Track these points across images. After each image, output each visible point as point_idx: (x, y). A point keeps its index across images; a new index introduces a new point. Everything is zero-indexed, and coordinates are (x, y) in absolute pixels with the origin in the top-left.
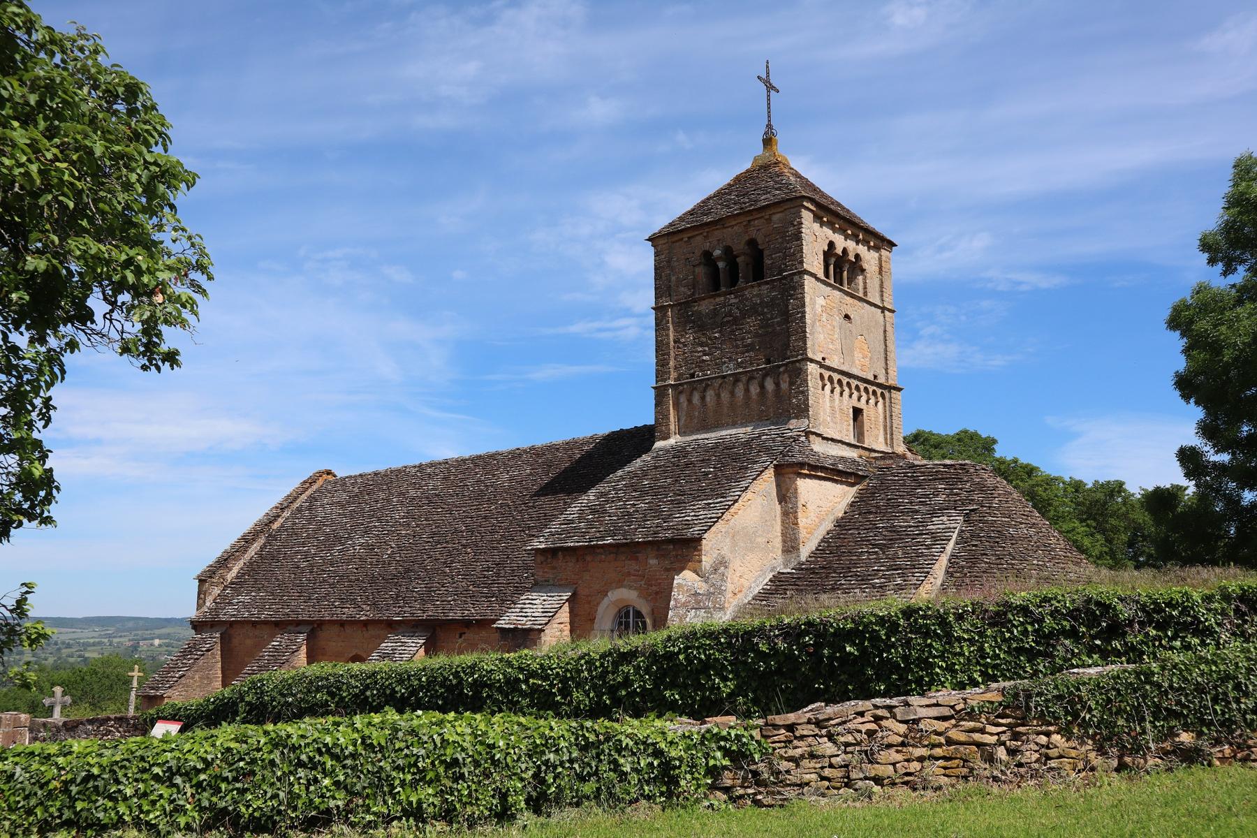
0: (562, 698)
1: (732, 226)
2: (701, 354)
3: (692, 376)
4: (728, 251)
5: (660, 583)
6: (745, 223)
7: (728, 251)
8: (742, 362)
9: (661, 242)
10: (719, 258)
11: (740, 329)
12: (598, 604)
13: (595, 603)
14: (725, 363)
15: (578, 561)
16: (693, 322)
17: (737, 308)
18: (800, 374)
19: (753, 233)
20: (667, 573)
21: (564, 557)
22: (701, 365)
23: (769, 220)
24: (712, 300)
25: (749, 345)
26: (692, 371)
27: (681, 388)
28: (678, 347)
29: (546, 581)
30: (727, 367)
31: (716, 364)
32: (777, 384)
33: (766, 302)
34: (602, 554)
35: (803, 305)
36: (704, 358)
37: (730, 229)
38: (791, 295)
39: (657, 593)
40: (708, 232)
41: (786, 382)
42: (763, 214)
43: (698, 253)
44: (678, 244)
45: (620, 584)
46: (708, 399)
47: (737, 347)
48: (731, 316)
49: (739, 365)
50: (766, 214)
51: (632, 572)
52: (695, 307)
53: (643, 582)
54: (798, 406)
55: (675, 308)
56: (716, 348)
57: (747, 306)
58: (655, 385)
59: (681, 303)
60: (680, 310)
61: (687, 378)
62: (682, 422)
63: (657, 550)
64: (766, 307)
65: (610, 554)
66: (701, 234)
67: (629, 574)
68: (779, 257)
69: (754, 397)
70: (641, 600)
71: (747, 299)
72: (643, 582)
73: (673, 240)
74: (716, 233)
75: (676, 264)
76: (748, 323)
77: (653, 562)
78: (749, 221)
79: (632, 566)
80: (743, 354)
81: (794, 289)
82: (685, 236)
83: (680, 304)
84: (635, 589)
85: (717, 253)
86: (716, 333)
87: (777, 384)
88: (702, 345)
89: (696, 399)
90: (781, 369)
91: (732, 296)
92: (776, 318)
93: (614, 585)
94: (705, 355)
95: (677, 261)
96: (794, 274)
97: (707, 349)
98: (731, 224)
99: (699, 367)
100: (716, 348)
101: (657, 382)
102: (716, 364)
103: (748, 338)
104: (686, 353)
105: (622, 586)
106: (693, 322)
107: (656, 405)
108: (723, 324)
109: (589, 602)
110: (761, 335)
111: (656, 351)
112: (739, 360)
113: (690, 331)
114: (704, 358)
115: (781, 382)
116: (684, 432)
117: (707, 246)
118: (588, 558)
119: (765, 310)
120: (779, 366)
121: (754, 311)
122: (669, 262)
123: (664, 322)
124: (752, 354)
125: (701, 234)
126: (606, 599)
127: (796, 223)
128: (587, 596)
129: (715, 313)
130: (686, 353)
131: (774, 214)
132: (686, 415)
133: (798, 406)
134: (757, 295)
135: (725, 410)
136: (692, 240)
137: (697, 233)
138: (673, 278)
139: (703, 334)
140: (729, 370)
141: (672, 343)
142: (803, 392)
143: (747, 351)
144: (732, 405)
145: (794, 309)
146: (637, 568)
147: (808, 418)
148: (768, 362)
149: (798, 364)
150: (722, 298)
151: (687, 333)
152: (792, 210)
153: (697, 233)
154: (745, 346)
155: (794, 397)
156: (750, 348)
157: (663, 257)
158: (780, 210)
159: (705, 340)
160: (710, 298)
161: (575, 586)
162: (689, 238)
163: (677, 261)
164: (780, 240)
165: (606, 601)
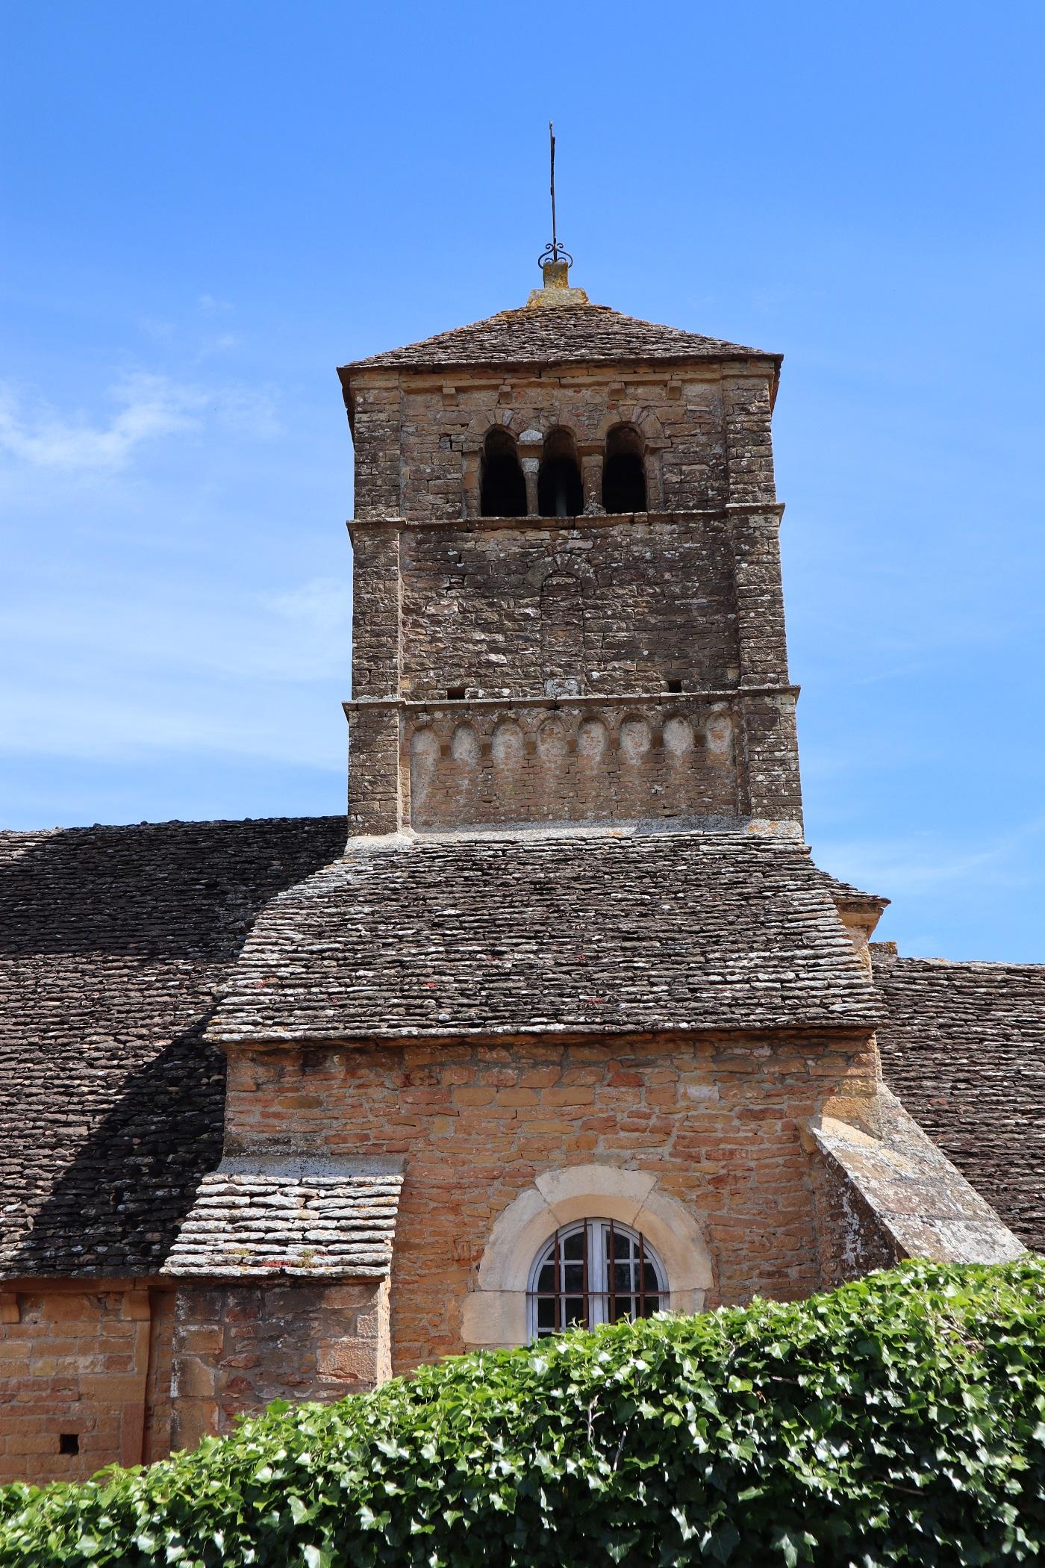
0: (196, 1549)
1: (578, 387)
2: (484, 647)
3: (456, 693)
4: (558, 435)
5: (732, 1153)
6: (616, 386)
7: (558, 435)
8: (602, 680)
9: (378, 384)
10: (531, 449)
11: (596, 607)
12: (496, 1211)
13: (482, 1208)
14: (553, 675)
15: (408, 1082)
16: (463, 574)
17: (588, 561)
18: (773, 722)
19: (630, 411)
20: (753, 1125)
21: (352, 1072)
22: (481, 671)
23: (675, 392)
24: (516, 534)
25: (620, 645)
26: (457, 683)
27: (424, 717)
28: (416, 624)
29: (276, 1142)
30: (560, 685)
31: (527, 676)
32: (700, 740)
33: (667, 560)
34: (505, 1065)
35: (776, 579)
36: (493, 657)
37: (570, 392)
38: (743, 554)
39: (718, 1181)
40: (513, 386)
41: (720, 737)
42: (666, 377)
43: (478, 429)
44: (420, 398)
45: (581, 1153)
46: (499, 752)
47: (587, 643)
48: (569, 575)
49: (593, 685)
50: (675, 377)
51: (622, 1118)
52: (466, 540)
53: (666, 1150)
54: (772, 792)
55: (409, 536)
56: (527, 639)
57: (616, 560)
58: (349, 700)
59: (432, 527)
60: (420, 543)
61: (442, 697)
62: (422, 797)
63: (714, 1059)
64: (670, 570)
65: (534, 1066)
66: (496, 387)
67: (610, 1125)
68: (702, 472)
69: (635, 762)
70: (666, 1200)
71: (617, 546)
72: (666, 1150)
73: (413, 385)
74: (533, 392)
75: (413, 440)
76: (619, 597)
77: (701, 1091)
78: (626, 383)
79: (628, 1102)
80: (606, 661)
81: (752, 541)
82: (449, 385)
83: (425, 528)
84: (642, 1167)
85: (532, 435)
86: (527, 606)
87: (700, 740)
88: (486, 627)
89: (465, 747)
90: (717, 707)
91: (575, 533)
92: (695, 596)
93: (557, 1155)
94: (497, 650)
95: (418, 433)
96: (754, 510)
97: (500, 638)
98: (577, 381)
99: (478, 675)
100: (527, 639)
101: (355, 694)
102: (527, 676)
103: (620, 629)
104: (440, 640)
105: (591, 1159)
106: (463, 574)
107: (354, 749)
108: (545, 591)
109: (456, 1209)
110: (654, 628)
111: (356, 623)
112: (595, 675)
113: (453, 593)
114: (493, 657)
115: (709, 737)
116: (426, 823)
117: (504, 416)
118: (450, 1076)
119: (667, 576)
120: (710, 700)
121: (635, 571)
122: (398, 429)
123: (382, 559)
124: (629, 665)
125: (496, 387)
126: (527, 1197)
127: (753, 409)
128: (448, 1189)
129: (524, 562)
130: (440, 640)
131: (692, 381)
132: (432, 783)
133: (772, 792)
134: (645, 542)
135: (551, 784)
136: (462, 397)
137: (477, 382)
138: (405, 470)
139: (491, 605)
140: (571, 689)
141: (400, 614)
142: (782, 762)
143: (617, 658)
144: (570, 773)
145: (750, 583)
146: (643, 1107)
147: (800, 820)
148: (674, 686)
149: (767, 700)
150: (546, 535)
151: (440, 596)
152: (741, 382)
153: (477, 382)
154: (610, 646)
155: (760, 771)
156: (626, 650)
157: (383, 416)
158: (709, 376)
159: (495, 617)
160: (511, 528)
161: (403, 1157)
162: (459, 390)
163: (418, 433)
164: (703, 439)
165: (527, 1203)
